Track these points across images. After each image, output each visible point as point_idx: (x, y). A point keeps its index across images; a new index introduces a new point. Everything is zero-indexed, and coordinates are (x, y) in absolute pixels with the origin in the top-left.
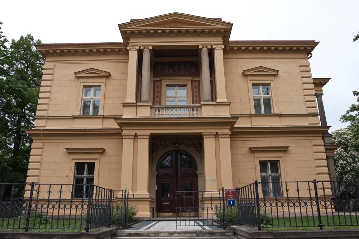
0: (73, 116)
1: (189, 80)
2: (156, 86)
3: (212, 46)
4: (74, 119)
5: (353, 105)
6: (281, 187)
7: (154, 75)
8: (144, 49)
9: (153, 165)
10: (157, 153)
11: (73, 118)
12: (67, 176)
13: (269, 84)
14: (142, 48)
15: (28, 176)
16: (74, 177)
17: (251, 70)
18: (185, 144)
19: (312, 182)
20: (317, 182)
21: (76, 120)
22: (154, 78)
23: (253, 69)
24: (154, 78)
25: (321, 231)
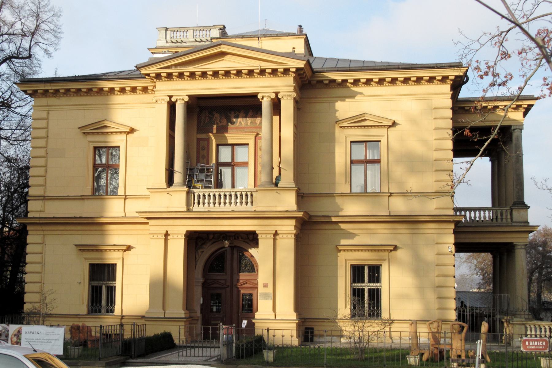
0: (81, 196)
1: (252, 137)
2: (201, 147)
3: (277, 93)
4: (83, 199)
5: (263, 284)
6: (166, 355)
7: (198, 129)
8: (177, 101)
9: (197, 267)
10: (203, 252)
11: (82, 198)
12: (80, 283)
13: (380, 141)
14: (173, 100)
15: (26, 293)
16: (89, 284)
17: (347, 120)
18: (242, 238)
19: (266, 330)
20: (270, 330)
21: (86, 201)
22: (198, 133)
23: (352, 119)
24: (198, 133)
25: (535, 338)
